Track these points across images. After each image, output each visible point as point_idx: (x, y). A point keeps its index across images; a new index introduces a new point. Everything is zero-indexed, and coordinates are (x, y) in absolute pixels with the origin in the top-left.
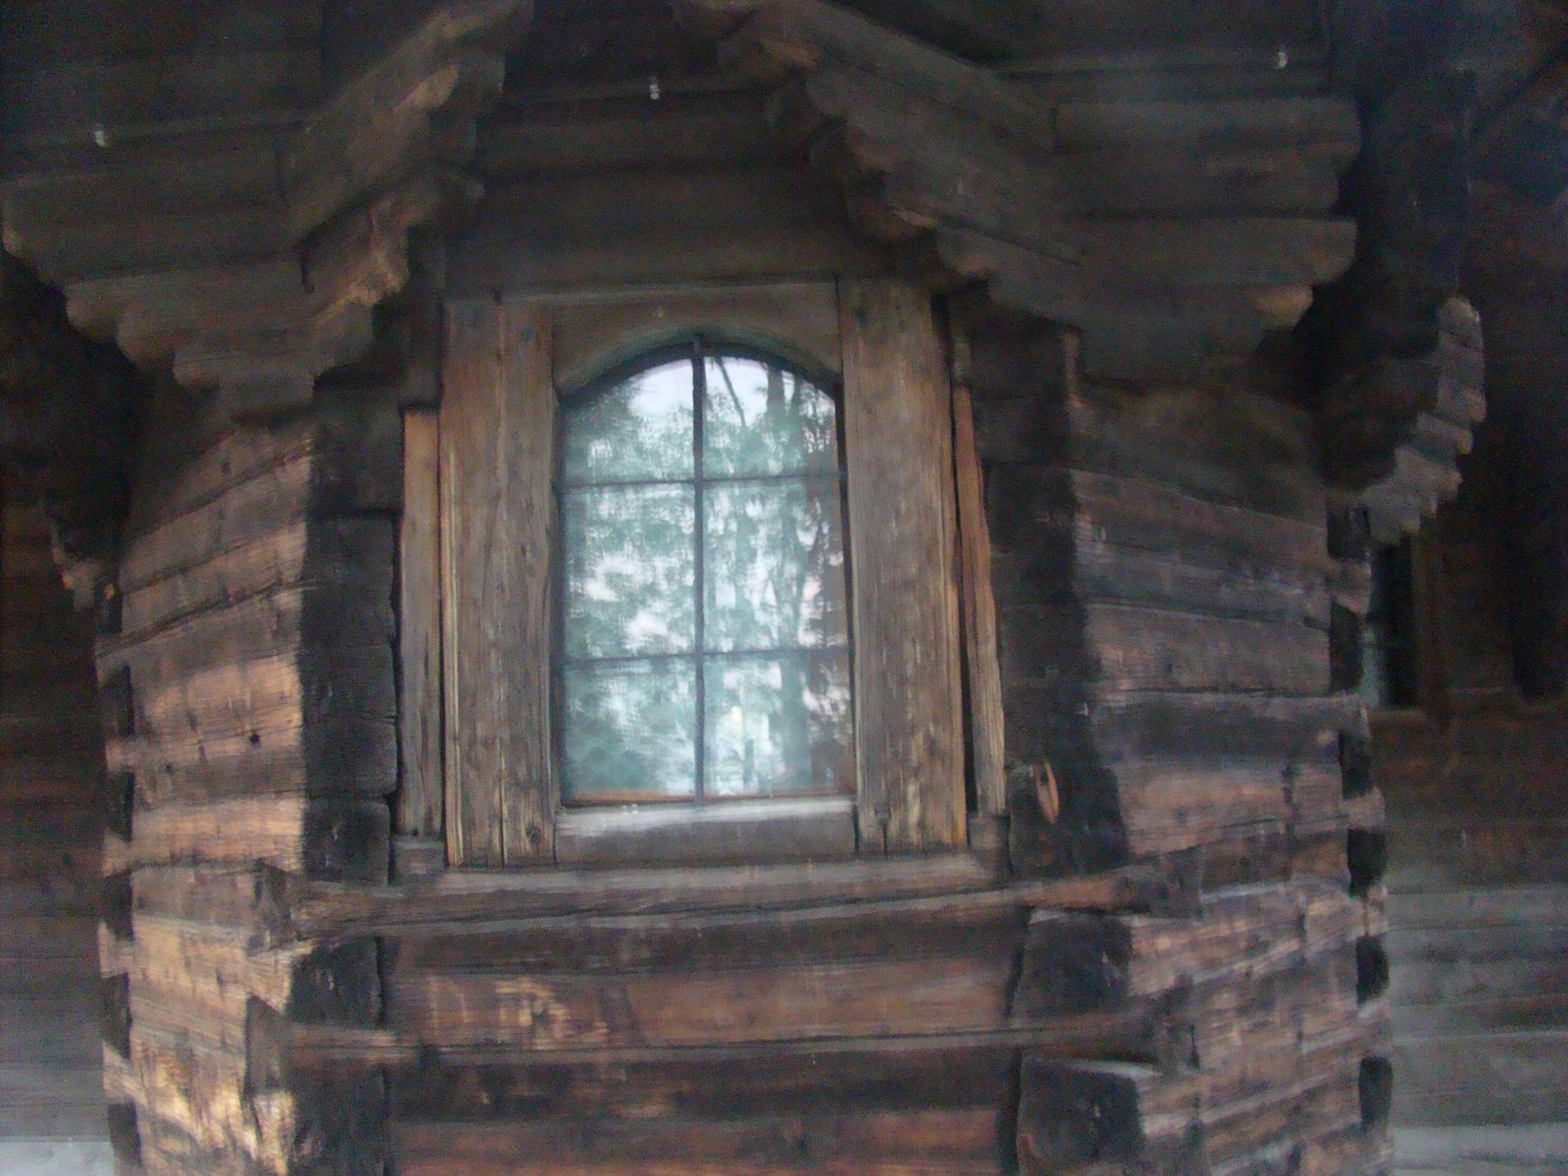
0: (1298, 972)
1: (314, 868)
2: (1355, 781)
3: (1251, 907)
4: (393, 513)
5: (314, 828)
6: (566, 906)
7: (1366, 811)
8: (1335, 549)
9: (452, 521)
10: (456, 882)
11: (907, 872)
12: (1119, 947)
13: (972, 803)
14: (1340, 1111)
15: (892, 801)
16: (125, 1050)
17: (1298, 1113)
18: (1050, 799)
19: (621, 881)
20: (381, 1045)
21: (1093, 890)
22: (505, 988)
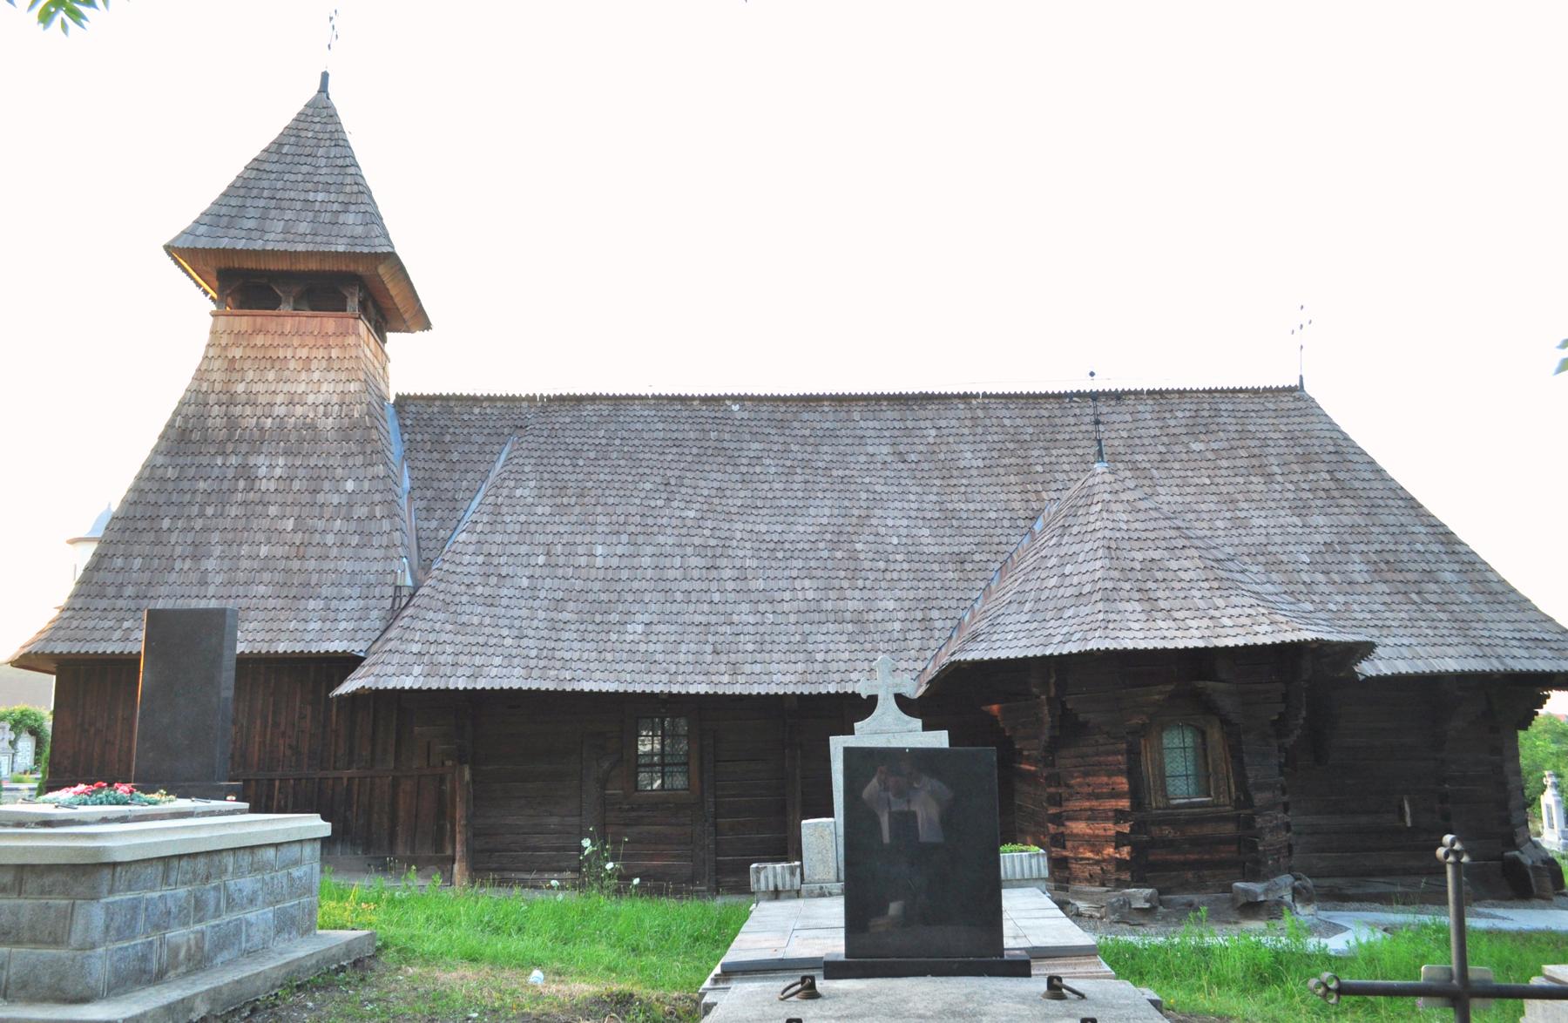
0: (1277, 827)
1: (1133, 810)
2: (1284, 793)
3: (1270, 815)
4: (1140, 753)
5: (1132, 806)
6: (1172, 814)
7: (1286, 798)
8: (1279, 751)
9: (1149, 755)
10: (1154, 812)
11: (1222, 809)
12: (1254, 821)
13: (1230, 798)
14: (1285, 852)
15: (1218, 798)
16: (348, 663)
17: (1278, 851)
18: (1242, 798)
19: (1180, 811)
20: (1145, 837)
21: (1249, 811)
22: (1164, 827)
